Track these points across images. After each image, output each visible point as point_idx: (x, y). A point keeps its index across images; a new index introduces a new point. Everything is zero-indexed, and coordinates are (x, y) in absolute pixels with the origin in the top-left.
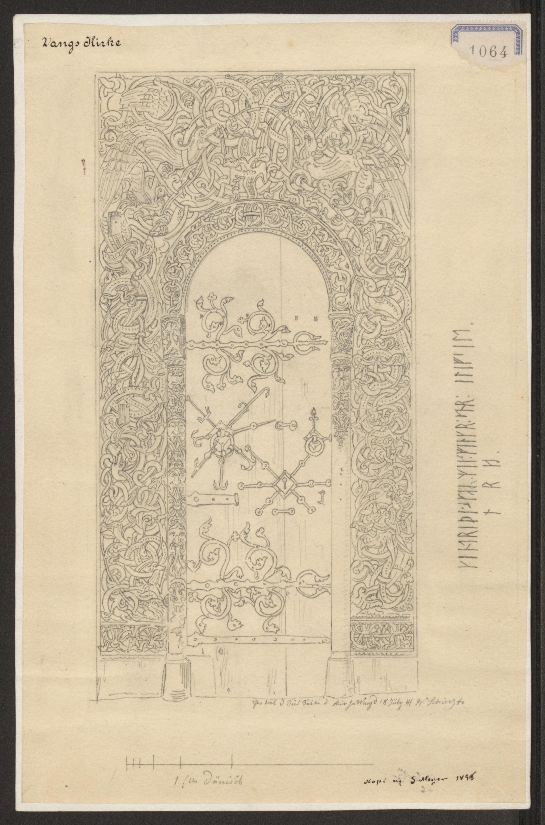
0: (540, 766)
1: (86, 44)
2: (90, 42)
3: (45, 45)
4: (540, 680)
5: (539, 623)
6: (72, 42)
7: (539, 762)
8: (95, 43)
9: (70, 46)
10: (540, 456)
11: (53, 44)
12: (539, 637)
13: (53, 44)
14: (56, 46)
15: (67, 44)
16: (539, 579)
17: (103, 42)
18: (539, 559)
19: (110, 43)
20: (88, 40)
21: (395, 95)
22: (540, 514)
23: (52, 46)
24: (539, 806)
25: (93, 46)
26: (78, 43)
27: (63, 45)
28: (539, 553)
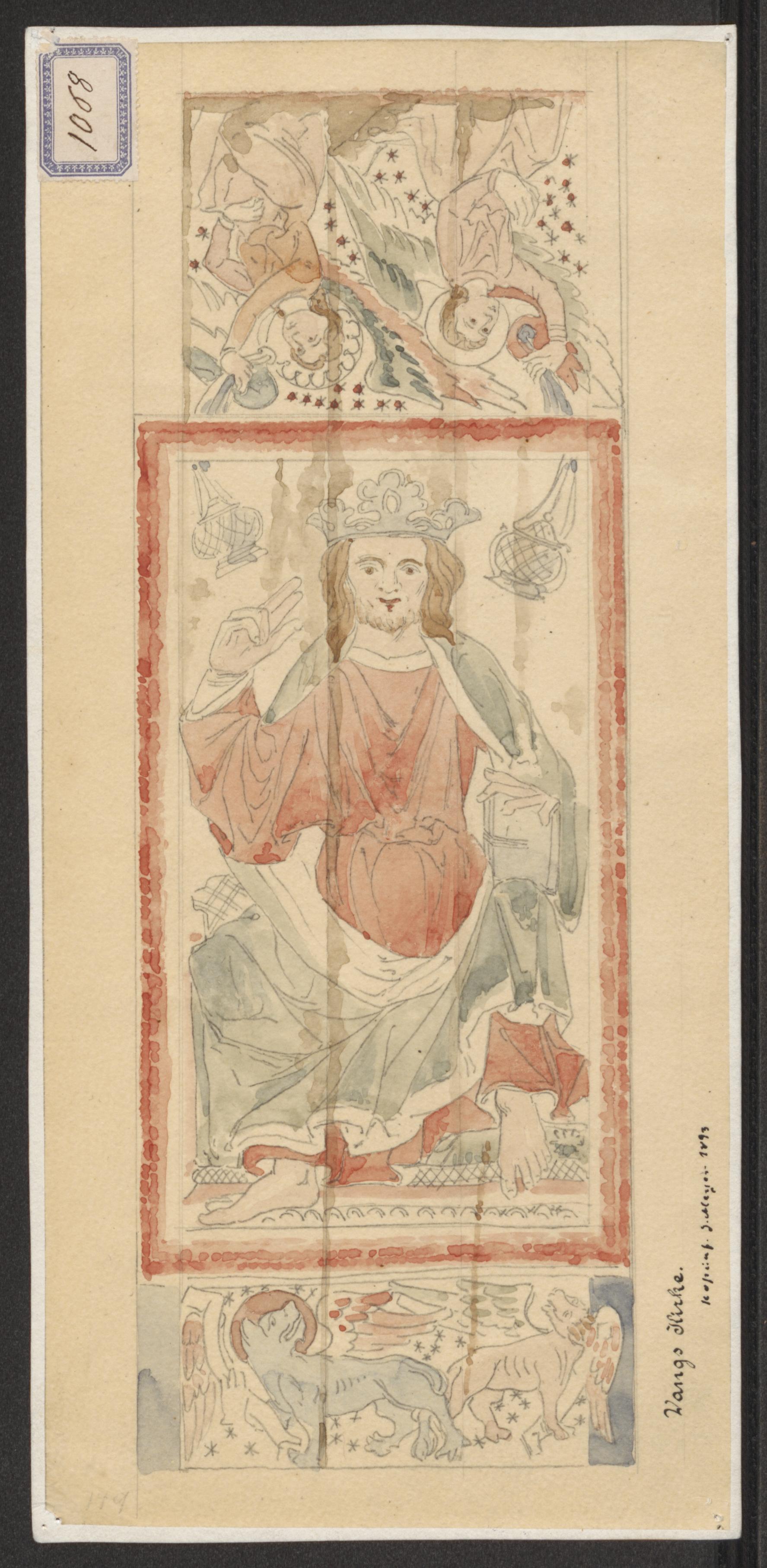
0: (757, 1122)
1: (679, 1331)
2: (677, 1326)
3: (678, 1411)
4: (756, 959)
5: (756, 855)
6: (675, 1363)
7: (756, 1116)
8: (677, 1318)
9: (682, 1366)
10: (758, 543)
11: (678, 1396)
12: (756, 805)
13: (678, 1396)
14: (682, 1391)
15: (678, 1371)
16: (756, 773)
17: (676, 1304)
18: (756, 736)
19: (678, 1293)
20: (672, 1328)
21: (547, 406)
22: (757, 652)
23: (680, 1399)
24: (756, 1196)
25: (681, 1321)
26: (676, 1350)
27: (681, 1379)
28: (756, 724)
